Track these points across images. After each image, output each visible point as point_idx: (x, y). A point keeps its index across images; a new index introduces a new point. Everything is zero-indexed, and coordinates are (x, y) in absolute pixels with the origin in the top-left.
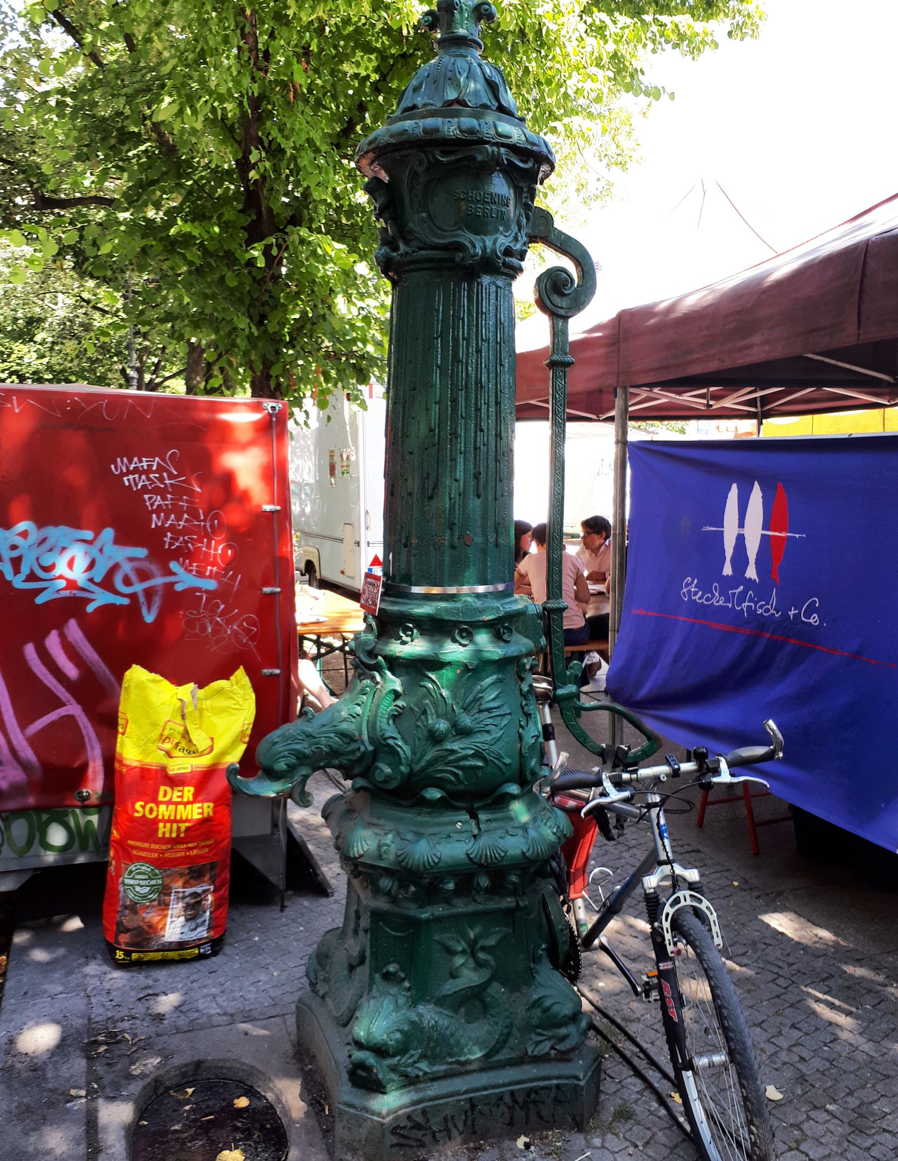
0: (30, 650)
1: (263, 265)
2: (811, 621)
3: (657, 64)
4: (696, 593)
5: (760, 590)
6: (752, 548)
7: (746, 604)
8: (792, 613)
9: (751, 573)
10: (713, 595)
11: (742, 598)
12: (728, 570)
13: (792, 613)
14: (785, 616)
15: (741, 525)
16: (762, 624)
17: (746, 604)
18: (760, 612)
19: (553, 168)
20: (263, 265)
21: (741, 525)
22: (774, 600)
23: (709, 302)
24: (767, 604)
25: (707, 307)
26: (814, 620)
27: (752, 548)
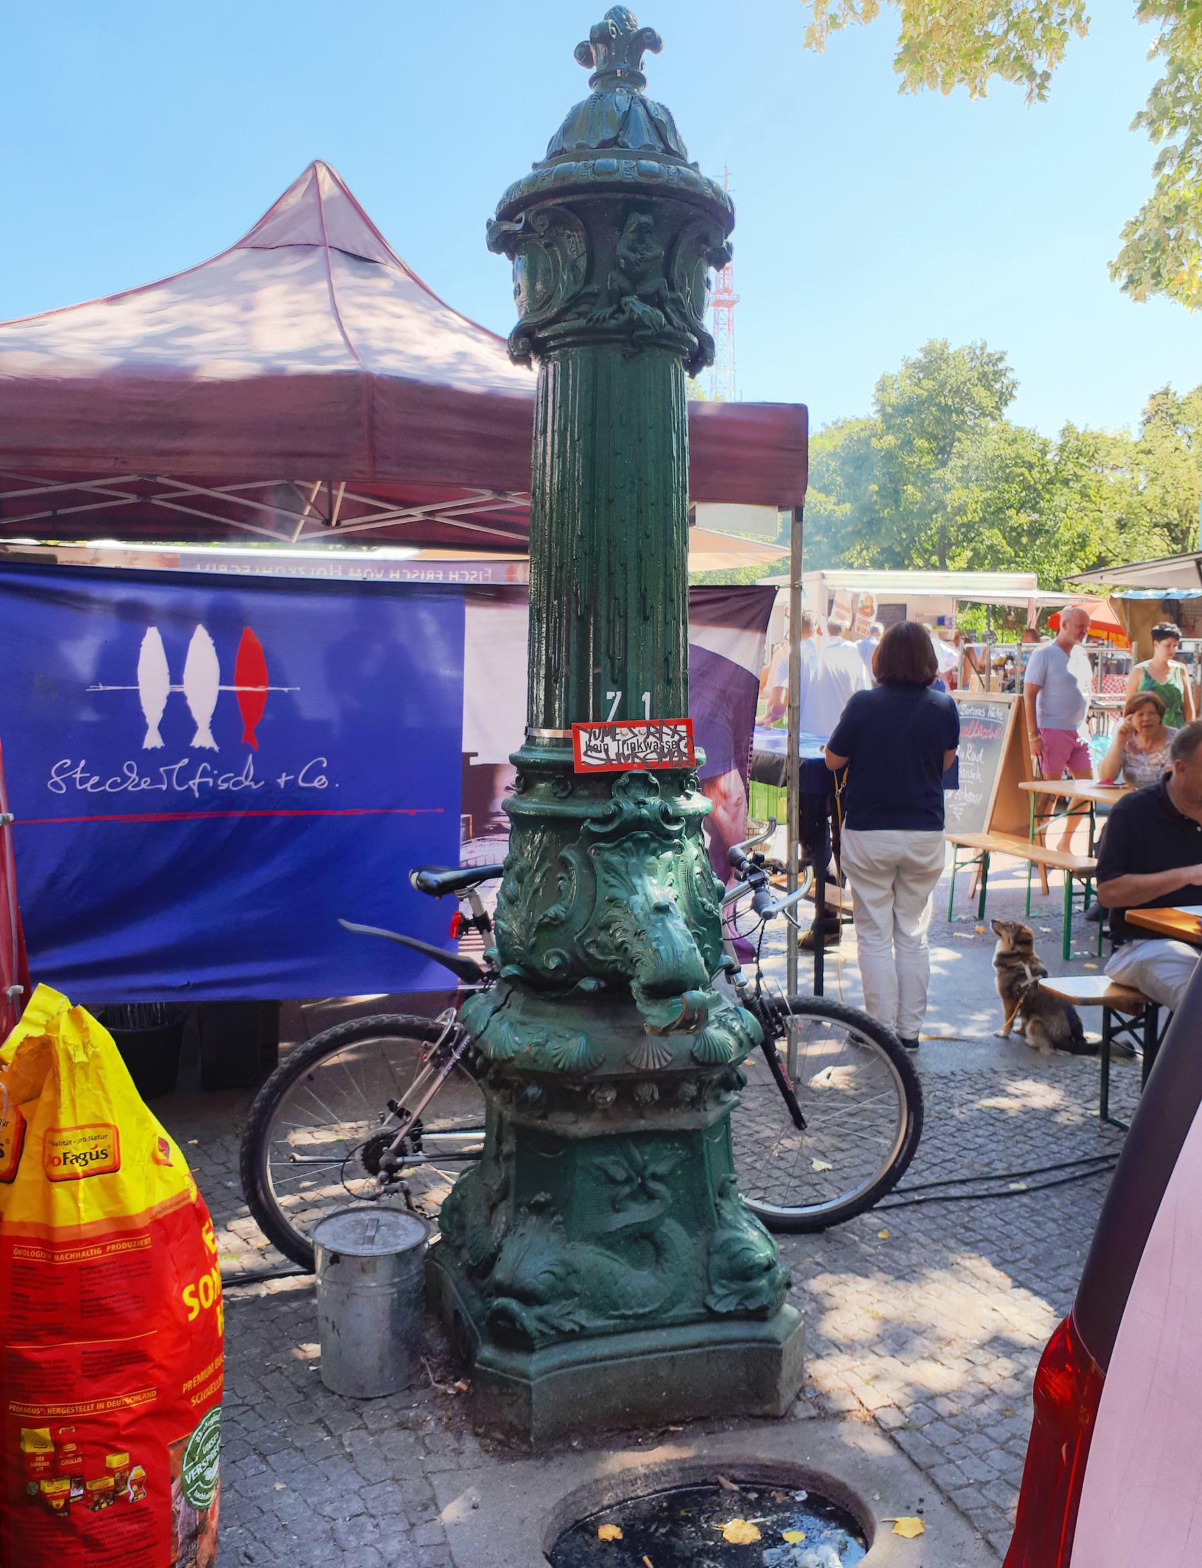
0: (520, 571)
1: (318, 1347)
2: (316, 784)
3: (1123, 244)
4: (83, 781)
5: (224, 760)
6: (202, 706)
7: (197, 780)
8: (282, 781)
9: (203, 739)
10: (125, 779)
11: (186, 775)
12: (153, 740)
13: (282, 781)
14: (271, 786)
15: (176, 675)
16: (230, 800)
17: (197, 780)
18: (224, 786)
19: (1156, 92)
20: (318, 1347)
21: (176, 675)
22: (250, 766)
23: (67, 376)
24: (238, 774)
25: (70, 380)
26: (320, 782)
27: (202, 706)
